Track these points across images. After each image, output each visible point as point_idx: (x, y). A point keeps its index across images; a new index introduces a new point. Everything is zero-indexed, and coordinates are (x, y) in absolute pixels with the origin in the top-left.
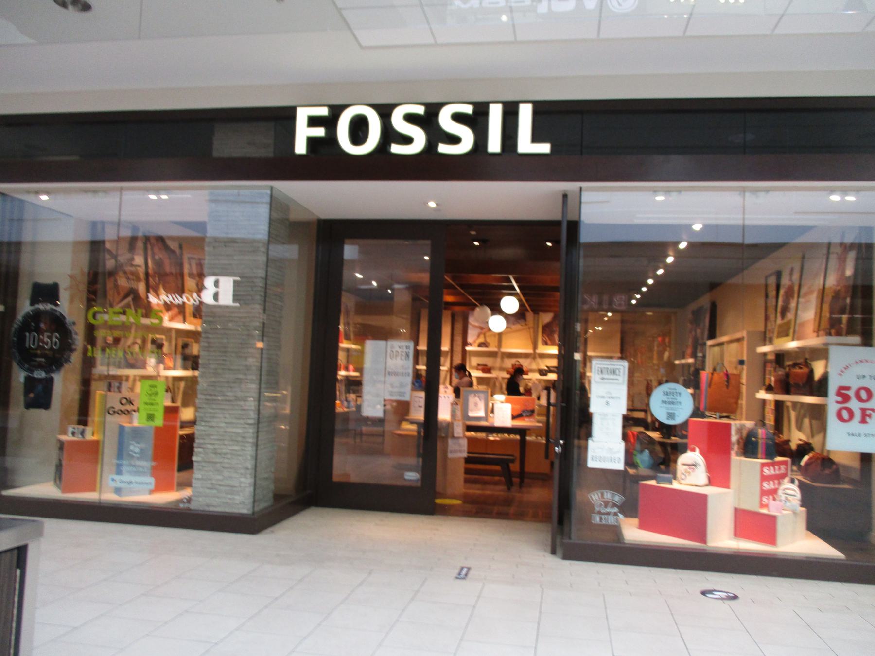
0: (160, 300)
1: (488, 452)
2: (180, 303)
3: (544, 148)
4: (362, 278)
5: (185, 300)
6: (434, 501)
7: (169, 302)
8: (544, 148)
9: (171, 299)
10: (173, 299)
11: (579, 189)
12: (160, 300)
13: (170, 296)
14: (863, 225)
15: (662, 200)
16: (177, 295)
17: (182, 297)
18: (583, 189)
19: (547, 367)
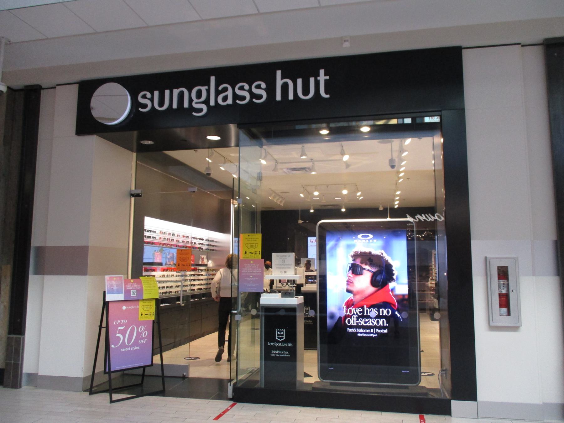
0: (416, 219)
1: (127, 248)
2: (433, 220)
3: (328, 96)
4: (404, 174)
5: (436, 218)
6: (113, 345)
7: (423, 220)
8: (328, 96)
9: (424, 218)
10: (426, 217)
11: (241, 143)
12: (416, 219)
13: (423, 215)
14: (28, 372)
15: (219, 140)
16: (429, 214)
17: (434, 216)
18: (138, 198)
19: (350, 285)
